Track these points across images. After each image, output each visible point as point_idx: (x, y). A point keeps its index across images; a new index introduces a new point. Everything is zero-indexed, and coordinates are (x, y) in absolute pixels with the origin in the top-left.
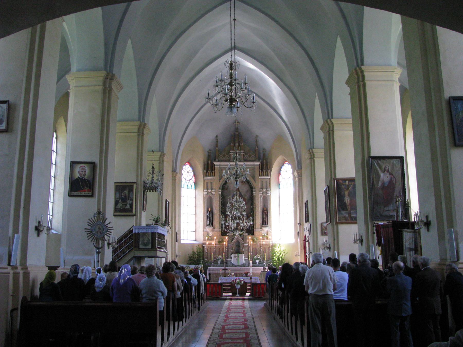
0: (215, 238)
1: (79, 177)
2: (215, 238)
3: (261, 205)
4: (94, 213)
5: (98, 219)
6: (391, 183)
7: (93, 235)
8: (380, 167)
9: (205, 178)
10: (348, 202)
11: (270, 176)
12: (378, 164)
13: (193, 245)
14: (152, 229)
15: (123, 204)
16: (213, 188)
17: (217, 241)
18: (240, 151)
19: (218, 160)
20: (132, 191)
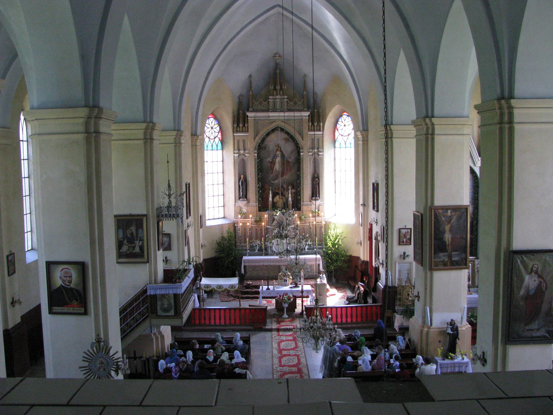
0: (251, 216)
1: (61, 285)
2: (251, 216)
3: (310, 171)
4: (91, 343)
5: (98, 350)
7: (93, 374)
8: (525, 267)
9: (235, 135)
11: (323, 131)
12: (523, 262)
13: (221, 226)
14: (174, 290)
15: (129, 247)
16: (246, 147)
17: (253, 220)
18: (282, 97)
19: (252, 110)
20: (142, 227)
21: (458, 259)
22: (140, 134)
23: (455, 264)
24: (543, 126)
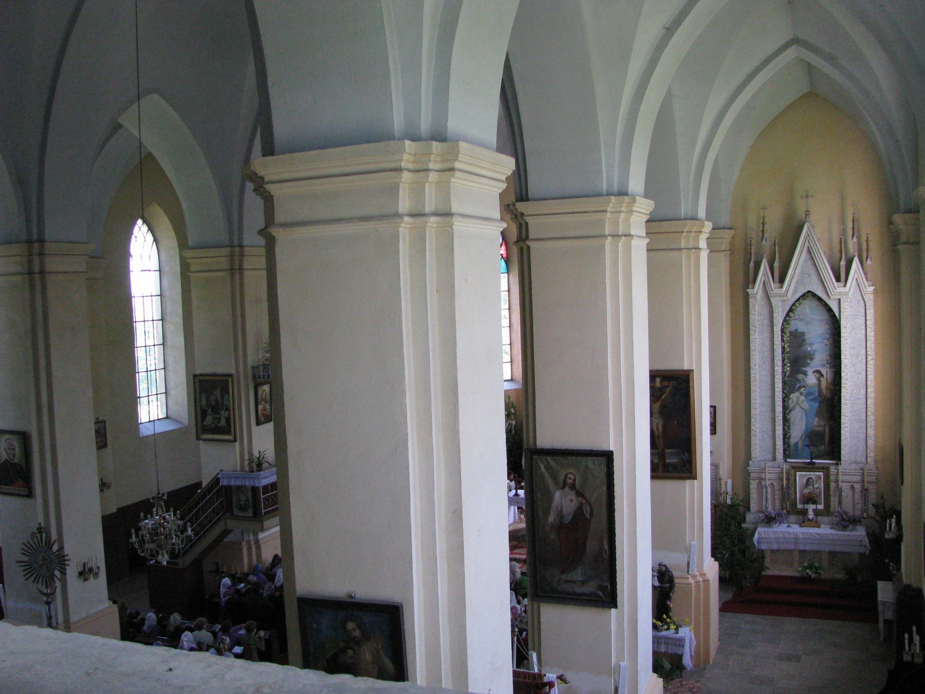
1: (6, 459)
6: (580, 520)
10: (658, 429)
12: (548, 468)
15: (214, 418)
20: (228, 392)
21: (676, 461)
22: (224, 263)
23: (671, 470)
24: (576, 243)
